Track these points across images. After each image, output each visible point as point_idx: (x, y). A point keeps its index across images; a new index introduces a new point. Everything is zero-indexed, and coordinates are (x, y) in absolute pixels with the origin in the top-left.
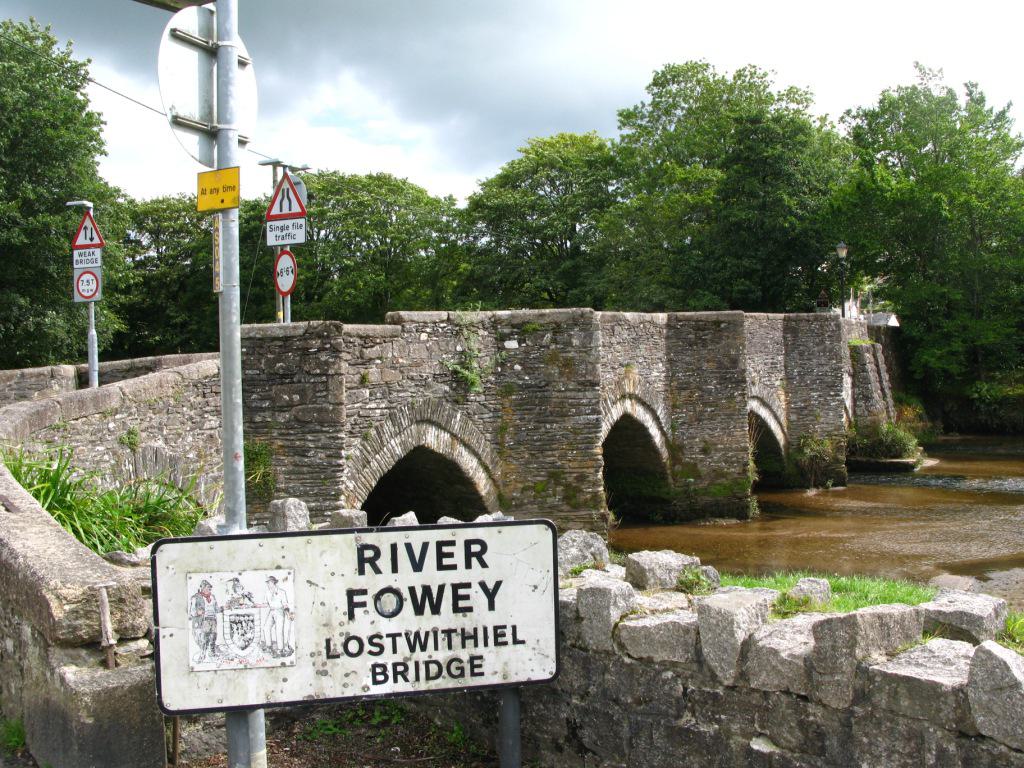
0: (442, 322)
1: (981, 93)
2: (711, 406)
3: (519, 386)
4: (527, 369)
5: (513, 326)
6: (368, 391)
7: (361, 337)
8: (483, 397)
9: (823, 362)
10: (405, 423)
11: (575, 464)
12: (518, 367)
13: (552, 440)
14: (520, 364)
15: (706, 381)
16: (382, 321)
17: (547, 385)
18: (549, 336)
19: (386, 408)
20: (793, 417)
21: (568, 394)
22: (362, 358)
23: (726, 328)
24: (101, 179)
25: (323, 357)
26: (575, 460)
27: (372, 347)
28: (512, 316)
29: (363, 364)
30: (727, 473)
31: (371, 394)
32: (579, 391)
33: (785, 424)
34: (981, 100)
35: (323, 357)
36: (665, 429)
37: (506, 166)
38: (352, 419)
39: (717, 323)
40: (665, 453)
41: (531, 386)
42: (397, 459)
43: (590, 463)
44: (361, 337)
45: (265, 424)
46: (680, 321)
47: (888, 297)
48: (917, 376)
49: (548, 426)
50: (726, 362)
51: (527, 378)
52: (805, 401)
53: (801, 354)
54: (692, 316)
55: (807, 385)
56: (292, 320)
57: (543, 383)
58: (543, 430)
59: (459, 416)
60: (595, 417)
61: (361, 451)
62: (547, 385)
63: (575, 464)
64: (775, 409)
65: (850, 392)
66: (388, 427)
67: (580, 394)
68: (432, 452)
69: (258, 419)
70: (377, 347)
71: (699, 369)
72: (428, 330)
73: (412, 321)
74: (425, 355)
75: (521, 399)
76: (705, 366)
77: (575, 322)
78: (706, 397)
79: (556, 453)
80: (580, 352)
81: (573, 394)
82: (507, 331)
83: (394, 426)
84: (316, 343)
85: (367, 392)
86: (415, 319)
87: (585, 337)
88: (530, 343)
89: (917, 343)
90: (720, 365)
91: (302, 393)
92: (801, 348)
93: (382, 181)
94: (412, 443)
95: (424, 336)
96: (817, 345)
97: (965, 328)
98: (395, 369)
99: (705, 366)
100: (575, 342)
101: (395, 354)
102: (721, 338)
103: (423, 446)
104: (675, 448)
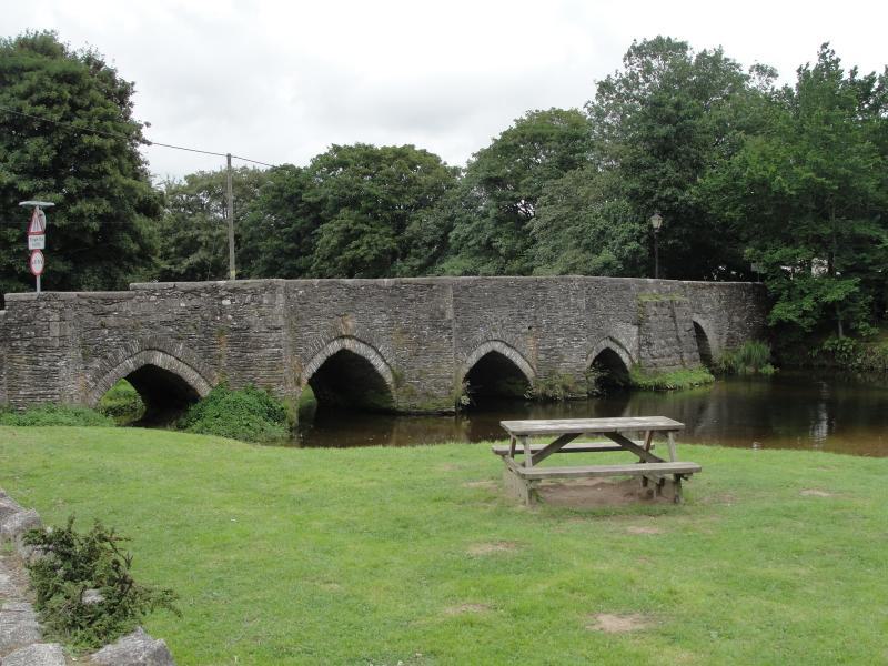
1: (186, 178)
4: (236, 318)
10: (136, 350)
12: (230, 317)
16: (128, 289)
18: (249, 297)
20: (542, 357)
24: (726, 59)
25: (47, 311)
35: (47, 311)
37: (499, 137)
39: (430, 286)
40: (389, 379)
41: (238, 329)
45: (17, 347)
50: (437, 315)
52: (552, 344)
53: (549, 308)
56: (42, 290)
66: (122, 351)
69: (14, 344)
74: (153, 310)
76: (421, 316)
79: (253, 372)
84: (43, 304)
85: (106, 331)
90: (432, 316)
91: (36, 331)
95: (153, 298)
99: (421, 316)
100: (265, 301)
102: (432, 296)
103: (152, 365)
104: (398, 379)
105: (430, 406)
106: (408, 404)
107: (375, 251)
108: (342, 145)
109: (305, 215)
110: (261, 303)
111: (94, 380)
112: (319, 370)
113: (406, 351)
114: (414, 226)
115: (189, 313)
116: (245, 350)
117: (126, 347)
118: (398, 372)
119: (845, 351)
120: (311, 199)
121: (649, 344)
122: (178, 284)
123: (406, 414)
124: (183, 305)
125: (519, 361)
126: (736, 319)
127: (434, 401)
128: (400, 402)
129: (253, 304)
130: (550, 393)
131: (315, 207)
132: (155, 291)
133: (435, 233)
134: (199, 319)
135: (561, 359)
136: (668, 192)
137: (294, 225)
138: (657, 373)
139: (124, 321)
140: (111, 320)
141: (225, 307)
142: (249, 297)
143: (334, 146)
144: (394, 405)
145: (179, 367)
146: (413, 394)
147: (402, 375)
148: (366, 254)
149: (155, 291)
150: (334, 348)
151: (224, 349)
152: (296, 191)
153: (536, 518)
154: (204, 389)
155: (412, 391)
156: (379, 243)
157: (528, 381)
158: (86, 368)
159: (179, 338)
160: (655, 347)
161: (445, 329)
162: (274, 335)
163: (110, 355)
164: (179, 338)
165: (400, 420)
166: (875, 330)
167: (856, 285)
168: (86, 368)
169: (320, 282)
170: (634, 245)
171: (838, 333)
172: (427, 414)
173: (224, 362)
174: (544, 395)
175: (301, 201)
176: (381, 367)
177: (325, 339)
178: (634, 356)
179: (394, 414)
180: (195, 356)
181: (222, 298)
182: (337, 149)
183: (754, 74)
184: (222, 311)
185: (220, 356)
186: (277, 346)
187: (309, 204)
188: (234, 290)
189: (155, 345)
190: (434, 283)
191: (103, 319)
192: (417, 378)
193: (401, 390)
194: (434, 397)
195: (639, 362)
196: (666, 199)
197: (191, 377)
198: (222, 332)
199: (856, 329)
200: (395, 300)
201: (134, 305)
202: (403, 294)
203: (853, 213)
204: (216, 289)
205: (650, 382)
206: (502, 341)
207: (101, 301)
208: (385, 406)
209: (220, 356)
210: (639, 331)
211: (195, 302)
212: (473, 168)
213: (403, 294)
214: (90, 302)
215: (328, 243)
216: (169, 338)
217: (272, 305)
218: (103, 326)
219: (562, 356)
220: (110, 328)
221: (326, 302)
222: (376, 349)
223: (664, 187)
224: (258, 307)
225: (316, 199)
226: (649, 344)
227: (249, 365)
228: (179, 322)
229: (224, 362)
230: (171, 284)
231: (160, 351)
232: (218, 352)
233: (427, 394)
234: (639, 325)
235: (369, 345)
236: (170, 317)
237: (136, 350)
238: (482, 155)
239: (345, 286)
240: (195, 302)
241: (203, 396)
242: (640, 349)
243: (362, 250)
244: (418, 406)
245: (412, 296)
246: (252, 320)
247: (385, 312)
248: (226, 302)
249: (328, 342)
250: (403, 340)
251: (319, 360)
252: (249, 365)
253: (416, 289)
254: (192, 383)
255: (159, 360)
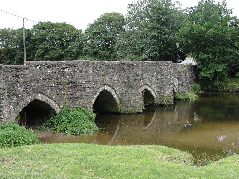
0: (44, 64)
2: (131, 87)
3: (69, 82)
4: (71, 77)
5: (67, 65)
6: (18, 84)
7: (16, 69)
8: (57, 85)
9: (167, 75)
10: (31, 93)
11: (84, 104)
12: (68, 77)
13: (78, 97)
14: (69, 76)
15: (130, 80)
17: (76, 82)
18: (77, 68)
19: (24, 89)
20: (159, 90)
21: (82, 84)
22: (17, 74)
23: (135, 66)
26: (84, 103)
27: (20, 71)
28: (66, 62)
29: (17, 76)
30: (135, 106)
31: (19, 85)
32: (85, 83)
33: (156, 92)
34: (225, 5)
36: (117, 94)
37: (97, 20)
38: (13, 92)
39: (133, 64)
40: (118, 100)
42: (28, 103)
43: (88, 104)
44: (16, 69)
46: (123, 64)
47: (135, 54)
48: (201, 78)
49: (77, 93)
51: (70, 80)
53: (161, 73)
54: (126, 62)
55: (162, 82)
57: (75, 81)
58: (75, 94)
59: (49, 91)
60: (90, 91)
61: (16, 101)
62: (76, 82)
63: (84, 104)
64: (153, 88)
65: (177, 83)
66: (25, 94)
67: (86, 85)
68: (41, 101)
70: (22, 71)
71: (128, 77)
72: (39, 66)
73: (34, 64)
74: (38, 74)
75: (69, 86)
77: (85, 64)
78: (130, 85)
79: (79, 101)
80: (86, 72)
81: (84, 84)
82: (65, 66)
83: (27, 94)
86: (35, 63)
87: (87, 68)
88: (71, 70)
89: (200, 70)
90: (134, 76)
92: (161, 71)
93: (64, 25)
94: (34, 98)
95: (37, 68)
96: (166, 70)
97: (213, 66)
98: (28, 77)
100: (84, 70)
101: (27, 73)
103: (37, 99)
104: (120, 101)
105: (133, 110)
106: (125, 110)
107: (57, 55)
108: (43, 22)
109: (32, 43)
110: (82, 70)
111: (13, 108)
112: (97, 98)
113: (124, 90)
114: (70, 47)
115: (52, 75)
116: (75, 91)
117: (27, 91)
118: (120, 98)
119: (221, 86)
120: (34, 39)
121: (182, 85)
122: (47, 62)
123: (124, 114)
124: (49, 71)
125: (152, 92)
126: (191, 76)
127: (134, 108)
128: (122, 109)
129: (78, 71)
130: (162, 103)
131: (34, 41)
132: (38, 65)
133: (76, 49)
134: (56, 78)
135: (165, 91)
136: (166, 36)
137: (28, 47)
138: (185, 95)
139: (26, 79)
140: (20, 79)
141: (66, 72)
142: (77, 68)
143: (40, 22)
144: (119, 111)
145: (48, 100)
146: (126, 106)
147: (122, 99)
148: (54, 56)
149: (38, 65)
150: (101, 89)
151: (65, 91)
152: (29, 36)
153: (218, 164)
154: (58, 110)
155: (126, 105)
156: (58, 52)
157: (154, 99)
158: (10, 103)
159: (48, 87)
160: (184, 86)
161: (139, 81)
162: (88, 85)
163: (20, 96)
164: (48, 87)
165: (121, 117)
166: (229, 80)
167: (225, 66)
168: (10, 103)
169: (97, 62)
170: (154, 53)
171: (217, 80)
172: (132, 114)
173: (65, 97)
174: (160, 104)
175: (30, 39)
176: (115, 96)
177: (99, 85)
178: (177, 89)
179: (119, 114)
180: (54, 94)
181: (64, 69)
182: (41, 23)
183: (176, 4)
184: (64, 74)
185: (64, 94)
186: (89, 90)
187: (33, 40)
188: (70, 65)
189: (39, 90)
190: (134, 63)
191: (17, 78)
192: (128, 100)
193: (122, 105)
194: (134, 107)
195: (179, 91)
196: (165, 39)
197: (53, 104)
198: (64, 84)
199: (224, 79)
200: (119, 70)
201: (30, 72)
202: (122, 67)
203: (223, 45)
204: (61, 64)
205: (184, 97)
206: (148, 85)
207: (15, 70)
208: (114, 111)
209: (64, 94)
210: (179, 81)
211: (54, 70)
212: (88, 30)
213: (122, 67)
214: (11, 70)
215: (40, 51)
216: (44, 87)
217: (87, 72)
218: (17, 82)
219: (165, 90)
220: (20, 83)
221: (100, 70)
222: (114, 89)
223: (164, 34)
224: (81, 72)
225: (36, 38)
226: (182, 85)
227: (77, 98)
228: (48, 80)
229: (65, 97)
230: (44, 62)
231: (41, 93)
232: (63, 92)
233: (132, 106)
234: (178, 79)
235: (112, 87)
236: (44, 77)
237: (31, 93)
238: (91, 26)
239: (105, 64)
240: (54, 70)
241: (57, 112)
242: (179, 87)
243: (51, 54)
244: (128, 110)
245: (126, 68)
246: (78, 78)
247: (116, 74)
248: (66, 70)
249: (100, 87)
250: (122, 86)
251: (97, 94)
252: (77, 98)
253: (127, 66)
254: (53, 107)
255: (40, 97)
